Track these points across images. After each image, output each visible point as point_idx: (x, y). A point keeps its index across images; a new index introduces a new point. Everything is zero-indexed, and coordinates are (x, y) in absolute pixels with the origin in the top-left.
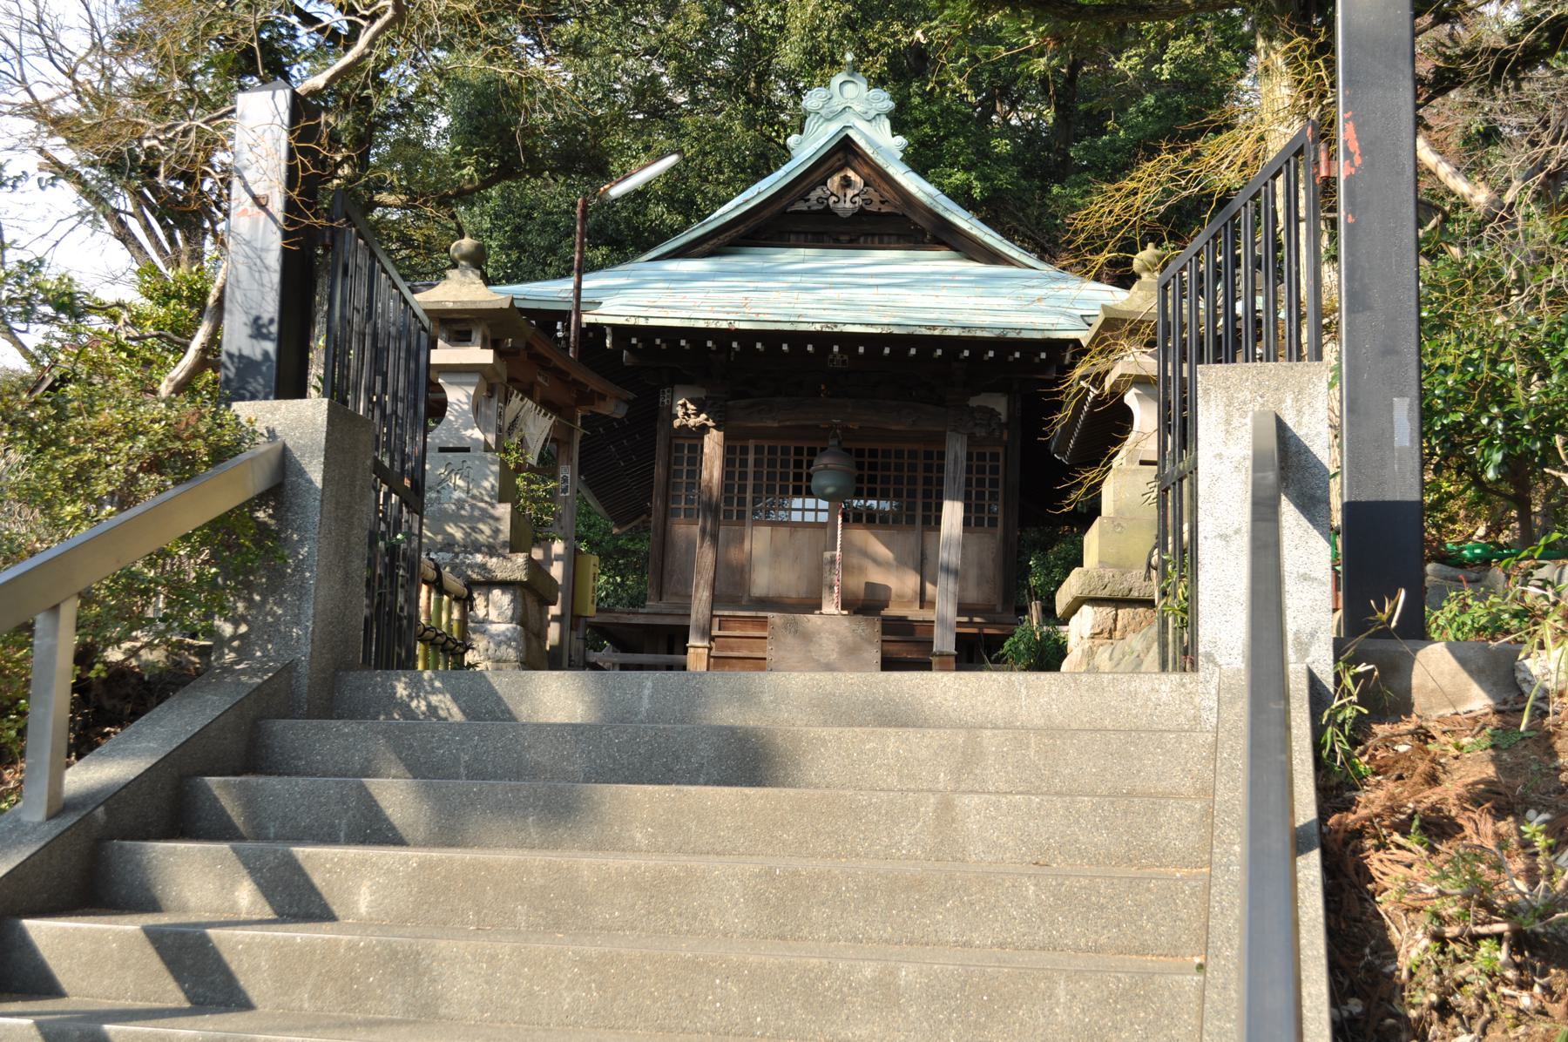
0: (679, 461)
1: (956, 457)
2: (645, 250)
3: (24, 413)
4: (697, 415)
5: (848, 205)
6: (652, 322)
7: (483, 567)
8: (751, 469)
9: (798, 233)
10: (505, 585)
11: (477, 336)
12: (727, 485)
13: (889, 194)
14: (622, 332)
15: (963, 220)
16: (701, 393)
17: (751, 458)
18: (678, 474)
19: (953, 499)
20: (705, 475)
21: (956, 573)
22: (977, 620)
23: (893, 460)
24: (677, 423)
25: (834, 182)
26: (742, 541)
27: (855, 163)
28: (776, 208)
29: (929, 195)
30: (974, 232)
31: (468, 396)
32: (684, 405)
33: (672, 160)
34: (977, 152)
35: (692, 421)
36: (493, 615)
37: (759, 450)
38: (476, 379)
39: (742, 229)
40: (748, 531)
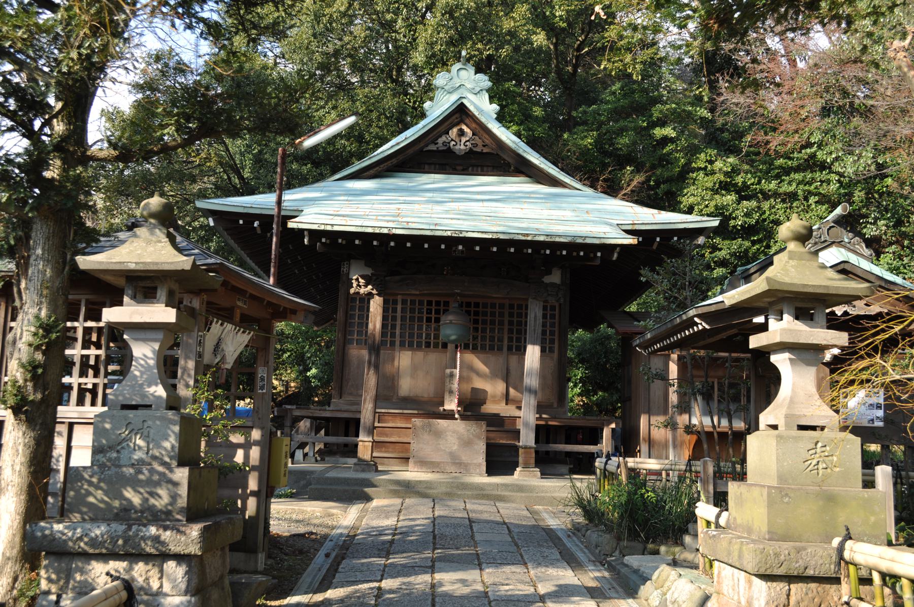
0: (353, 308)
1: (535, 316)
2: (334, 172)
3: (336, 100)
4: (366, 286)
5: (462, 147)
6: (336, 228)
7: (156, 539)
8: (399, 314)
9: (429, 164)
10: (179, 558)
11: (162, 294)
12: (383, 334)
13: (488, 141)
14: (315, 234)
15: (535, 158)
16: (368, 272)
17: (399, 307)
18: (353, 316)
19: (534, 344)
20: (370, 326)
21: (535, 393)
22: (544, 416)
23: (489, 310)
24: (352, 291)
25: (454, 132)
26: (393, 360)
27: (467, 121)
28: (417, 148)
29: (514, 142)
30: (542, 166)
31: (154, 351)
32: (357, 280)
33: (351, 120)
34: (523, 115)
35: (362, 291)
36: (167, 588)
37: (404, 302)
38: (160, 335)
39: (394, 161)
40: (397, 354)
